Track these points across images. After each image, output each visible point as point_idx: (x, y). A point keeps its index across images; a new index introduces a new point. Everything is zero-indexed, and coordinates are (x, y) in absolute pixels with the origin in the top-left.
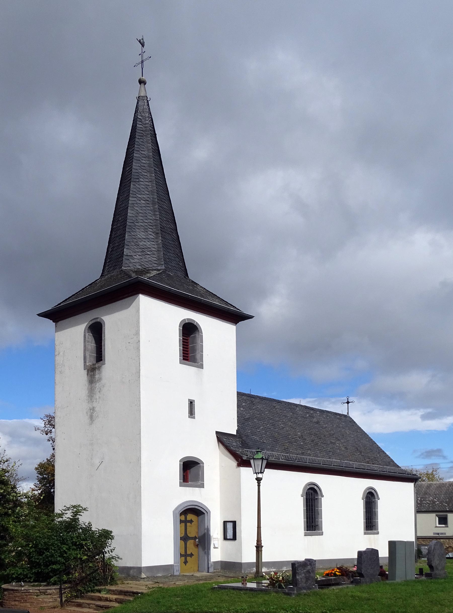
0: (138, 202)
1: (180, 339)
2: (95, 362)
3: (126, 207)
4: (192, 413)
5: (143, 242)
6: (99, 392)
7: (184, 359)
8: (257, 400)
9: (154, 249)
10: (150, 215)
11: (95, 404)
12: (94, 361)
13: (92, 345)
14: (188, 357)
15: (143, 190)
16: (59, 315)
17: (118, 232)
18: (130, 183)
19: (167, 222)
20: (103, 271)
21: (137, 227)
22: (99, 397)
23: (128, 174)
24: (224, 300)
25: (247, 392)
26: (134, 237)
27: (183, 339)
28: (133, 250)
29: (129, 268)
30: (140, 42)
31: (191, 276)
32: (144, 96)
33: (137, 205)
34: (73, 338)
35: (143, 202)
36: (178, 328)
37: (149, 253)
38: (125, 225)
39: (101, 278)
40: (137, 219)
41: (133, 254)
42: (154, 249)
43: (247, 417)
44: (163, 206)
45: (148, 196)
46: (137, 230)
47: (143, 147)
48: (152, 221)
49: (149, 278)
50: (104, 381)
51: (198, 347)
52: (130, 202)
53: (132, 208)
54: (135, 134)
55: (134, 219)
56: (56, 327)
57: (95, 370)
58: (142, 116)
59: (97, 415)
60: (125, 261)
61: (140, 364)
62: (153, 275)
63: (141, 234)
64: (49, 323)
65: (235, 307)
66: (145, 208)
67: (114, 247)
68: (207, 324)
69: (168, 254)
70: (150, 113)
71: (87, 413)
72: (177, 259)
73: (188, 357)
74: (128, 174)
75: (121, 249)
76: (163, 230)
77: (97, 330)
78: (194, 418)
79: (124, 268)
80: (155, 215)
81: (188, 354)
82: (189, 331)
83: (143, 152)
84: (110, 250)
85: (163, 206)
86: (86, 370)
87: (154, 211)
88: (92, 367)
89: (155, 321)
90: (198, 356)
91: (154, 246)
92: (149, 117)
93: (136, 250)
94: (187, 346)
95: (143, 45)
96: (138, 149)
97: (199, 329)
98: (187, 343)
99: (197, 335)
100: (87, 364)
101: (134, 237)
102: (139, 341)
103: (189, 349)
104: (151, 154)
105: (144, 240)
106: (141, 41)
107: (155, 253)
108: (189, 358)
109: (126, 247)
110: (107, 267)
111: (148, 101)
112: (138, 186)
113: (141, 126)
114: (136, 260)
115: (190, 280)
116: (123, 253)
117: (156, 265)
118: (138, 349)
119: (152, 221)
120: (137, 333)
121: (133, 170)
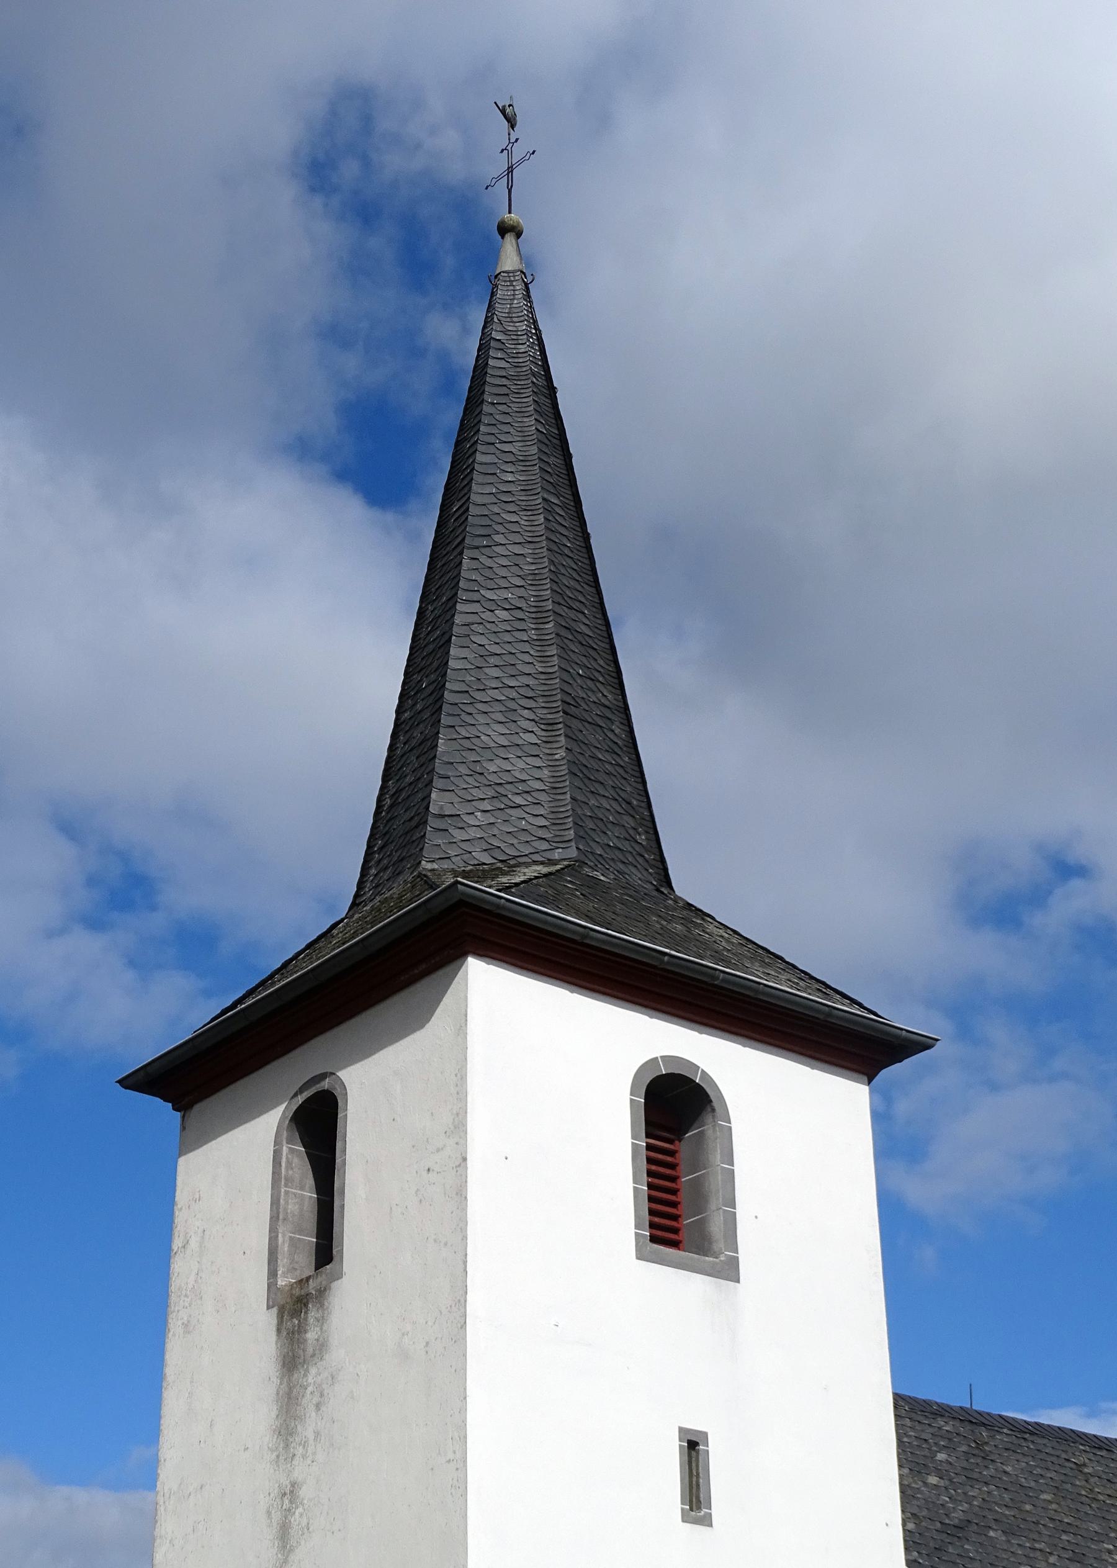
0: (488, 616)
1: (635, 1147)
2: (309, 1271)
3: (446, 637)
4: (695, 1498)
5: (498, 761)
6: (318, 1406)
7: (654, 1239)
8: (1003, 1438)
9: (538, 785)
10: (527, 658)
11: (300, 1470)
12: (305, 1261)
13: (303, 1195)
14: (676, 1231)
15: (503, 572)
16: (193, 1079)
17: (416, 733)
18: (461, 553)
19: (589, 682)
20: (361, 884)
21: (480, 706)
22: (317, 1434)
23: (456, 524)
24: (812, 978)
25: (956, 1398)
26: (467, 744)
27: (649, 1147)
28: (460, 793)
29: (446, 865)
30: (503, 111)
31: (684, 886)
32: (514, 272)
33: (480, 629)
34: (234, 1170)
35: (504, 615)
36: (627, 1097)
37: (519, 800)
38: (439, 704)
39: (352, 916)
40: (482, 676)
41: (461, 809)
42: (538, 785)
43: (957, 1516)
44: (573, 624)
45: (521, 592)
46: (482, 719)
47: (506, 428)
48: (531, 682)
49: (506, 889)
50: (337, 1355)
51: (715, 1182)
52: (458, 619)
53: (465, 641)
54: (483, 392)
55: (468, 678)
56: (183, 1128)
57: (306, 1305)
58: (505, 332)
59: (304, 1522)
60: (433, 838)
61: (465, 1262)
62: (522, 878)
63: (494, 734)
64: (159, 1109)
65: (860, 1005)
66: (507, 637)
67: (399, 791)
68: (740, 1073)
69: (592, 802)
70: (535, 322)
71: (269, 1513)
72: (628, 821)
73: (676, 1231)
74: (456, 524)
75: (420, 795)
76: (572, 710)
77: (318, 1127)
78: (707, 1521)
79: (429, 866)
80: (544, 658)
81: (676, 1218)
82: (674, 1108)
83: (506, 447)
84: (388, 801)
85: (573, 624)
86: (275, 1310)
87: (541, 642)
88: (297, 1292)
89: (530, 1066)
90: (716, 1226)
91: (537, 774)
92: (527, 333)
93: (474, 792)
94: (674, 1179)
95: (512, 122)
96: (491, 439)
97: (715, 1104)
98: (673, 1166)
99: (708, 1129)
100: (281, 1282)
101: (467, 744)
102: (465, 1159)
103: (684, 1197)
104: (534, 450)
105: (502, 753)
106: (508, 110)
107: (543, 797)
108: (684, 1235)
109: (438, 783)
110: (373, 871)
111: (526, 285)
112: (488, 562)
113: (503, 364)
114: (474, 833)
115: (677, 899)
116: (427, 808)
117: (545, 846)
118: (460, 1194)
119: (531, 682)
120: (459, 1127)
121: (473, 510)
